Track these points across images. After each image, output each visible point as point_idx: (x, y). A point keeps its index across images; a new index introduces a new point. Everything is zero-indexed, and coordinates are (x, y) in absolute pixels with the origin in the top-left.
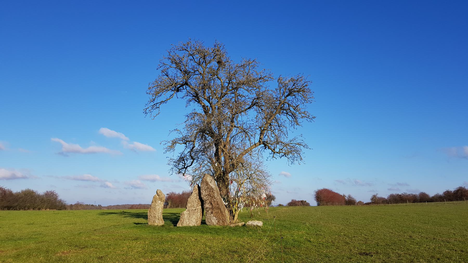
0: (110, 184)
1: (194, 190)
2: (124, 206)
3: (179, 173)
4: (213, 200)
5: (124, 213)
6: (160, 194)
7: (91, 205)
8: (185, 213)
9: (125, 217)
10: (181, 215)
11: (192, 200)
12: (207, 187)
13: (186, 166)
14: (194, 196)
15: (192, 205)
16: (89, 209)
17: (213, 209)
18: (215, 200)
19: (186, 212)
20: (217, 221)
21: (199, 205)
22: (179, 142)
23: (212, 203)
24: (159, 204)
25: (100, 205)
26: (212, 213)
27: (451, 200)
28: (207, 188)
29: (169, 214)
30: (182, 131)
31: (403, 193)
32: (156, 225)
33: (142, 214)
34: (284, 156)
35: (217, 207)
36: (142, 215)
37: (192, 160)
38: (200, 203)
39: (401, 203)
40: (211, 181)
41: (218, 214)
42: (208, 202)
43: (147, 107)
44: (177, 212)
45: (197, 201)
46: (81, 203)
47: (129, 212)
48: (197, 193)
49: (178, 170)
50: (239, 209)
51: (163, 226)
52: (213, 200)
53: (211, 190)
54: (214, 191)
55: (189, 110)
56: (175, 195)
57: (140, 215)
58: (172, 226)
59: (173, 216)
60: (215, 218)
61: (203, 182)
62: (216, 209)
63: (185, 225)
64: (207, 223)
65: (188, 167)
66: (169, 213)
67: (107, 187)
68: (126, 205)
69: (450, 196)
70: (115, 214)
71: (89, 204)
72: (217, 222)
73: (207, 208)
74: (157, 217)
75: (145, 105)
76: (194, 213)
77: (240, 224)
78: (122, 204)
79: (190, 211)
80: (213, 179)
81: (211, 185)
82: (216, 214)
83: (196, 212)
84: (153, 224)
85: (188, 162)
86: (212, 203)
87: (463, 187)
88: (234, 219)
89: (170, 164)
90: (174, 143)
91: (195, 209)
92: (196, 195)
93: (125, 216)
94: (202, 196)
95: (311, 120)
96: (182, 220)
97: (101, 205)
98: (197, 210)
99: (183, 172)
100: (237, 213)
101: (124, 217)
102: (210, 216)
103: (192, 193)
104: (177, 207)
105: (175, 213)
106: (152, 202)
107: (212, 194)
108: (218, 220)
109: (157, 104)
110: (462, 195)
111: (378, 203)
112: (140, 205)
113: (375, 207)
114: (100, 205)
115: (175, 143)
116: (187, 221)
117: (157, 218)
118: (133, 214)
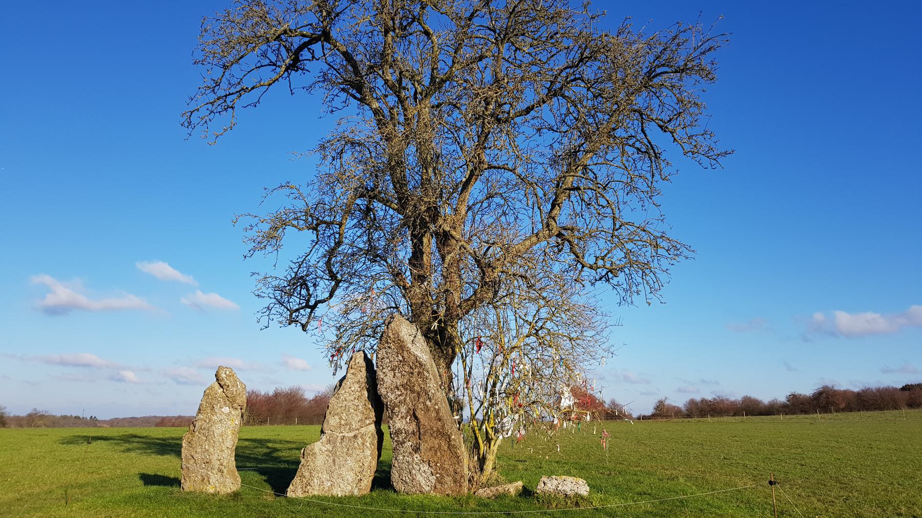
0: (129, 375)
1: (352, 371)
2: (132, 421)
3: (291, 321)
4: (421, 406)
5: (127, 439)
6: (228, 383)
7: (74, 416)
8: (317, 450)
9: (129, 450)
10: (302, 455)
11: (346, 402)
12: (401, 358)
13: (312, 303)
14: (353, 389)
15: (343, 422)
16: (71, 426)
17: (422, 437)
18: (428, 403)
19: (319, 447)
20: (433, 479)
21: (368, 422)
22: (295, 223)
23: (420, 414)
24: (224, 417)
25: (93, 417)
26: (417, 449)
27: (805, 411)
28: (401, 361)
29: (247, 443)
30: (305, 191)
31: (716, 397)
32: (211, 490)
33: (174, 441)
34: (604, 279)
35: (435, 429)
36: (175, 443)
37: (333, 283)
38: (374, 414)
39: (712, 416)
40: (412, 338)
41: (439, 454)
42: (403, 409)
43: (193, 107)
44: (267, 438)
45: (360, 407)
46: (41, 413)
47: (145, 434)
48: (364, 380)
49: (289, 313)
50: (501, 437)
51: (235, 496)
52: (421, 406)
53: (417, 370)
54: (425, 373)
55: (328, 129)
56: (257, 396)
57: (170, 445)
58: (268, 494)
59: (260, 450)
60: (426, 467)
61: (387, 343)
62: (432, 435)
63: (316, 493)
64: (398, 485)
65: (319, 305)
66: (246, 440)
67: (121, 380)
68: (150, 418)
69: (803, 404)
70: (103, 442)
71: (69, 415)
72: (434, 481)
73: (398, 432)
74: (216, 464)
75: (188, 101)
76: (350, 452)
77: (511, 490)
78: (142, 416)
79: (335, 443)
80: (419, 333)
81: (416, 353)
82: (430, 454)
83: (356, 444)
84: (199, 487)
85: (322, 291)
86: (419, 416)
87: (830, 386)
88: (482, 470)
89: (262, 294)
90: (280, 224)
91: (355, 437)
92: (357, 386)
93: (130, 447)
94: (382, 391)
95: (713, 162)
96: (307, 474)
97: (95, 417)
98: (360, 441)
99: (304, 321)
100: (494, 448)
101: (124, 452)
102: (410, 460)
103: (345, 381)
104: (263, 422)
105: (264, 438)
106: (199, 409)
107: (419, 385)
108: (438, 475)
109: (226, 96)
110: (827, 403)
111: (667, 416)
112: (179, 417)
113: (660, 425)
114: (93, 417)
115: (285, 224)
116: (325, 476)
117: (217, 466)
118: (152, 441)
